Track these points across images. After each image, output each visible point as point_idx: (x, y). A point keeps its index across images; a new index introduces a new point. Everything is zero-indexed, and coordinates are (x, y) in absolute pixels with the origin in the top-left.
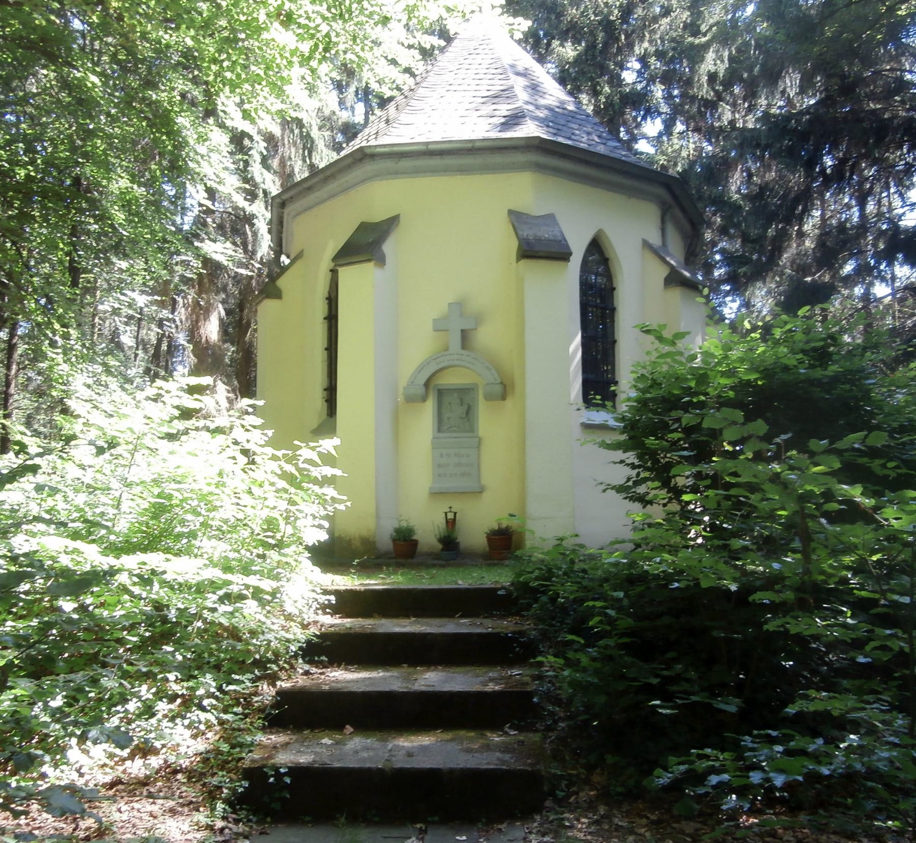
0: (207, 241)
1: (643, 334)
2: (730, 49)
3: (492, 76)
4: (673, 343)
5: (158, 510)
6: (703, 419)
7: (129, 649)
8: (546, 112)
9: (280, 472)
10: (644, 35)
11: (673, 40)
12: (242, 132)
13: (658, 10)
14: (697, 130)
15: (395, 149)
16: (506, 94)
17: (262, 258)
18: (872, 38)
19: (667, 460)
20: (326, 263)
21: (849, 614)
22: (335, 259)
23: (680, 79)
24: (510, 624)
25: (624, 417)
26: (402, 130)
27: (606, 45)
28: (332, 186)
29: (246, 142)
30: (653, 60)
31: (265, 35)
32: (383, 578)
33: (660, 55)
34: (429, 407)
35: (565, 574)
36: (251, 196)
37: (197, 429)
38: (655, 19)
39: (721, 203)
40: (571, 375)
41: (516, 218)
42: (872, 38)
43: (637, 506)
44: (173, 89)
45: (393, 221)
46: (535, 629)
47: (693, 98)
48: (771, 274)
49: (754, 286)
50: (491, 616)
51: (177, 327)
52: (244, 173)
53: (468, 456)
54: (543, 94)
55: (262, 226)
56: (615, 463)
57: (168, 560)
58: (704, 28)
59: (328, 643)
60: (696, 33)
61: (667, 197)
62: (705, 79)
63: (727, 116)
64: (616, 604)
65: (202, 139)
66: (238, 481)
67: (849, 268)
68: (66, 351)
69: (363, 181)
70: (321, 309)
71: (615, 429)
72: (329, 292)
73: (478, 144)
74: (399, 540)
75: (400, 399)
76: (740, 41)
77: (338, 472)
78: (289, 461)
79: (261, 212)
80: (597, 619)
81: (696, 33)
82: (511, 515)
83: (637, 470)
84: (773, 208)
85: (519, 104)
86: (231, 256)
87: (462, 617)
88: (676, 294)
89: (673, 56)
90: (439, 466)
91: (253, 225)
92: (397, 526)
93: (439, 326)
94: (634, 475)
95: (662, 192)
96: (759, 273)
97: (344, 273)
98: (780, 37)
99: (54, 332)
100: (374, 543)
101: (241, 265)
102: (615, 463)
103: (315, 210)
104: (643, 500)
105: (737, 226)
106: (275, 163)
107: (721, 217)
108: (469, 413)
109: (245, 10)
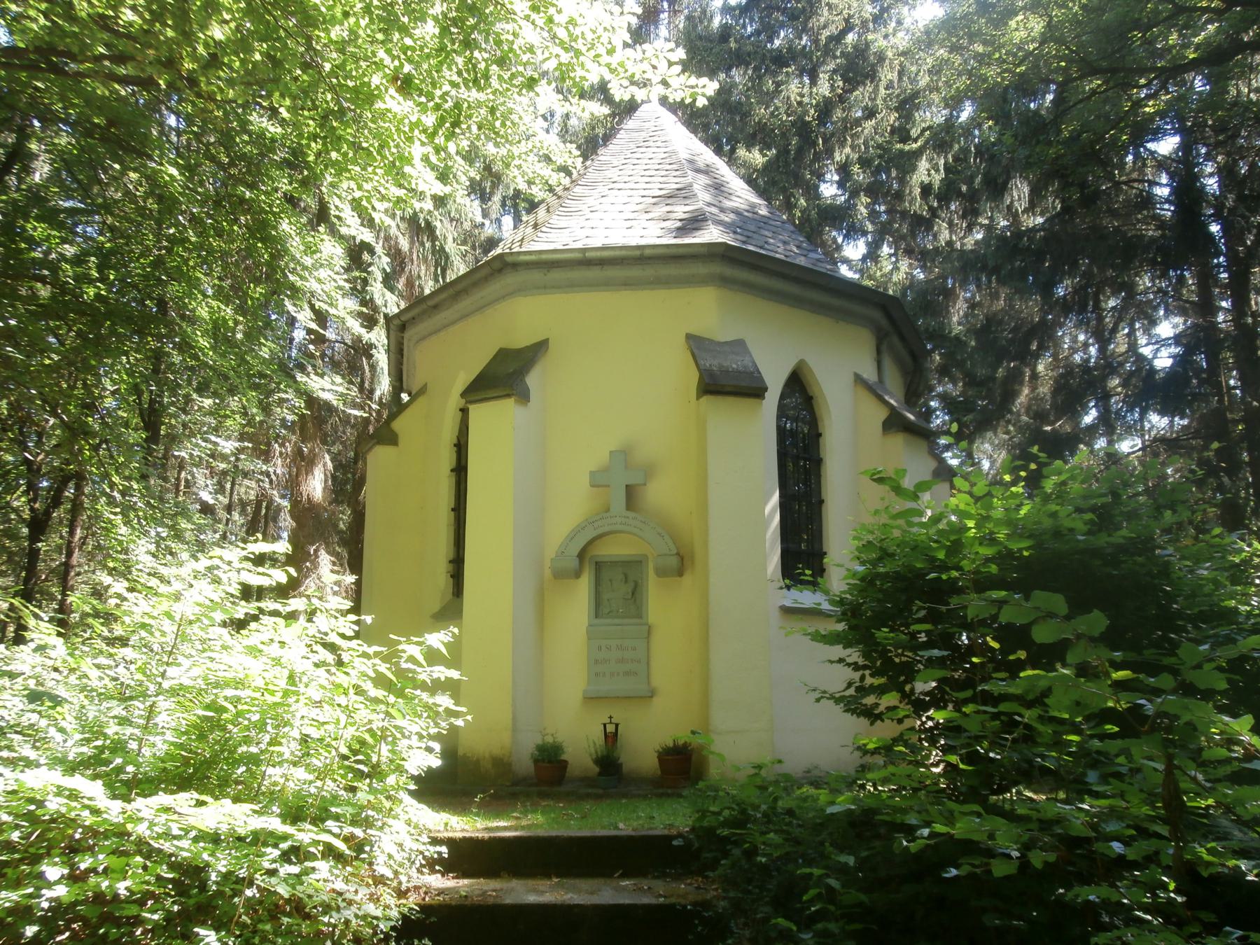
0: (312, 376)
1: (875, 484)
2: (945, 157)
3: (664, 173)
4: (915, 497)
5: (202, 730)
6: (1000, 608)
7: (149, 931)
8: (732, 216)
9: (373, 675)
10: (846, 140)
11: (879, 146)
12: (362, 242)
13: (859, 114)
14: (909, 252)
15: (544, 257)
16: (682, 194)
17: (381, 399)
18: (1115, 139)
19: (904, 659)
20: (454, 401)
21: (1172, 886)
22: (464, 394)
23: (888, 191)
24: (690, 888)
25: (842, 599)
26: (553, 235)
27: (800, 151)
28: (465, 304)
29: (366, 257)
30: (856, 169)
31: (379, 105)
32: (517, 818)
33: (864, 162)
34: (584, 584)
35: (765, 815)
36: (370, 322)
37: (275, 613)
38: (858, 122)
39: (940, 337)
40: (767, 545)
41: (696, 344)
42: (1115, 139)
43: (864, 721)
44: (276, 190)
45: (540, 348)
46: (724, 898)
47: (904, 214)
48: (1002, 423)
49: (984, 438)
50: (663, 876)
51: (271, 482)
52: (359, 290)
53: (634, 649)
54: (728, 196)
55: (382, 358)
56: (831, 662)
57: (200, 804)
58: (914, 133)
59: (433, 919)
60: (906, 138)
61: (884, 322)
62: (917, 191)
63: (945, 235)
64: (843, 870)
65: (310, 250)
66: (317, 683)
67: (1090, 418)
68: (127, 509)
69: (504, 297)
70: (447, 459)
71: (831, 616)
72: (458, 438)
73: (648, 252)
74: (543, 761)
75: (548, 573)
76: (956, 147)
77: (454, 674)
78: (386, 659)
79: (378, 337)
80: (812, 892)
81: (906, 138)
82: (693, 733)
83: (861, 672)
84: (1004, 342)
85: (700, 205)
86: (342, 395)
87: (625, 876)
88: (898, 441)
89: (880, 164)
90: (596, 661)
91: (372, 356)
92: (540, 742)
93: (598, 480)
94: (857, 679)
95: (877, 315)
96: (986, 423)
97: (476, 411)
98: (1008, 139)
99: (112, 485)
100: (510, 764)
101: (355, 406)
102: (831, 662)
103: (442, 333)
104: (872, 715)
105: (960, 365)
106: (401, 284)
107: (940, 354)
108: (636, 594)
109: (354, 73)
